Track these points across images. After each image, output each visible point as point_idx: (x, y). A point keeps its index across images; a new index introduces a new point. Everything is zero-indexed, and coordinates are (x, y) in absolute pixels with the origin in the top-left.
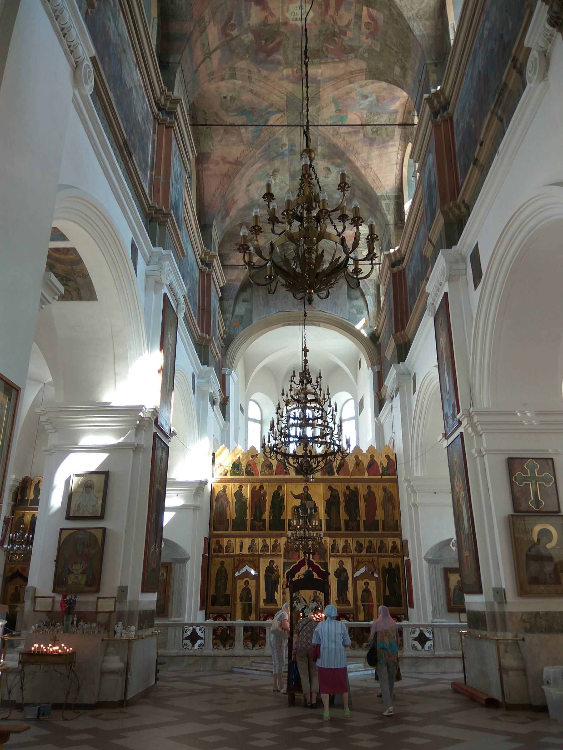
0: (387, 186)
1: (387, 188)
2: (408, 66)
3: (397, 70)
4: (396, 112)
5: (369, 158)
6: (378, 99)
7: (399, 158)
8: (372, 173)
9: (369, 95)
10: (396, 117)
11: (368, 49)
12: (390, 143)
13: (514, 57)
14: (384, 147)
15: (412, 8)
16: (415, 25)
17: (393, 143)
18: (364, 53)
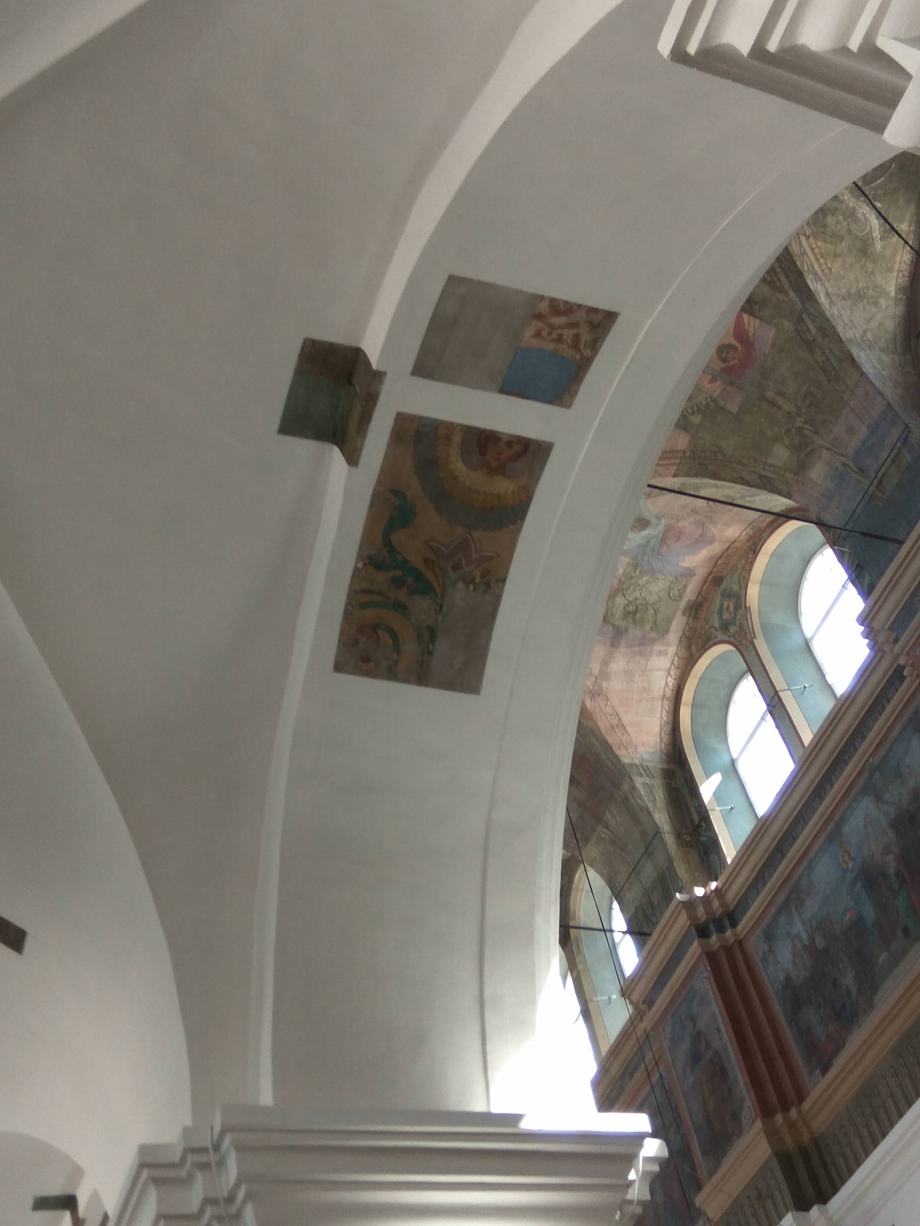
0: (643, 745)
1: (642, 750)
2: (818, 441)
3: (781, 454)
4: (689, 573)
5: (604, 674)
6: (664, 539)
7: (670, 685)
8: (609, 710)
9: (654, 521)
10: (685, 587)
11: (707, 406)
12: (657, 647)
14: (641, 653)
15: (854, 325)
16: (862, 354)
17: (663, 648)
18: (693, 413)
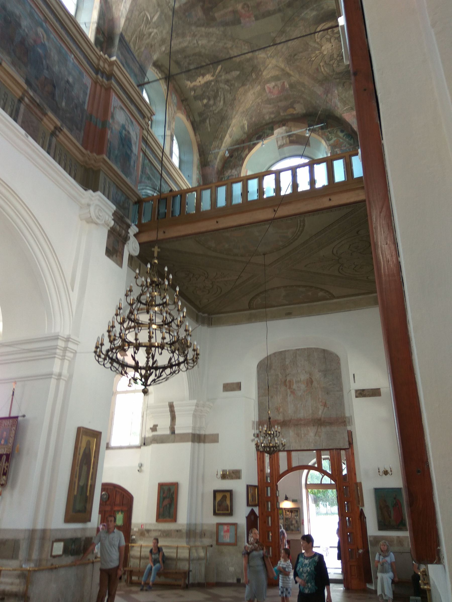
13: (61, 130)
